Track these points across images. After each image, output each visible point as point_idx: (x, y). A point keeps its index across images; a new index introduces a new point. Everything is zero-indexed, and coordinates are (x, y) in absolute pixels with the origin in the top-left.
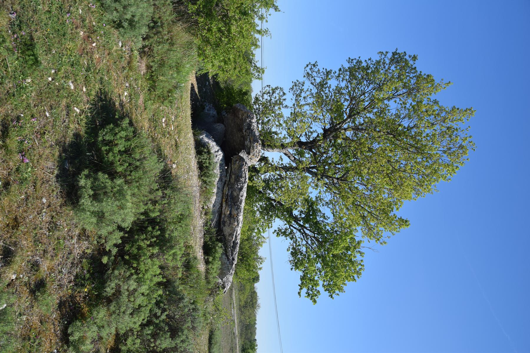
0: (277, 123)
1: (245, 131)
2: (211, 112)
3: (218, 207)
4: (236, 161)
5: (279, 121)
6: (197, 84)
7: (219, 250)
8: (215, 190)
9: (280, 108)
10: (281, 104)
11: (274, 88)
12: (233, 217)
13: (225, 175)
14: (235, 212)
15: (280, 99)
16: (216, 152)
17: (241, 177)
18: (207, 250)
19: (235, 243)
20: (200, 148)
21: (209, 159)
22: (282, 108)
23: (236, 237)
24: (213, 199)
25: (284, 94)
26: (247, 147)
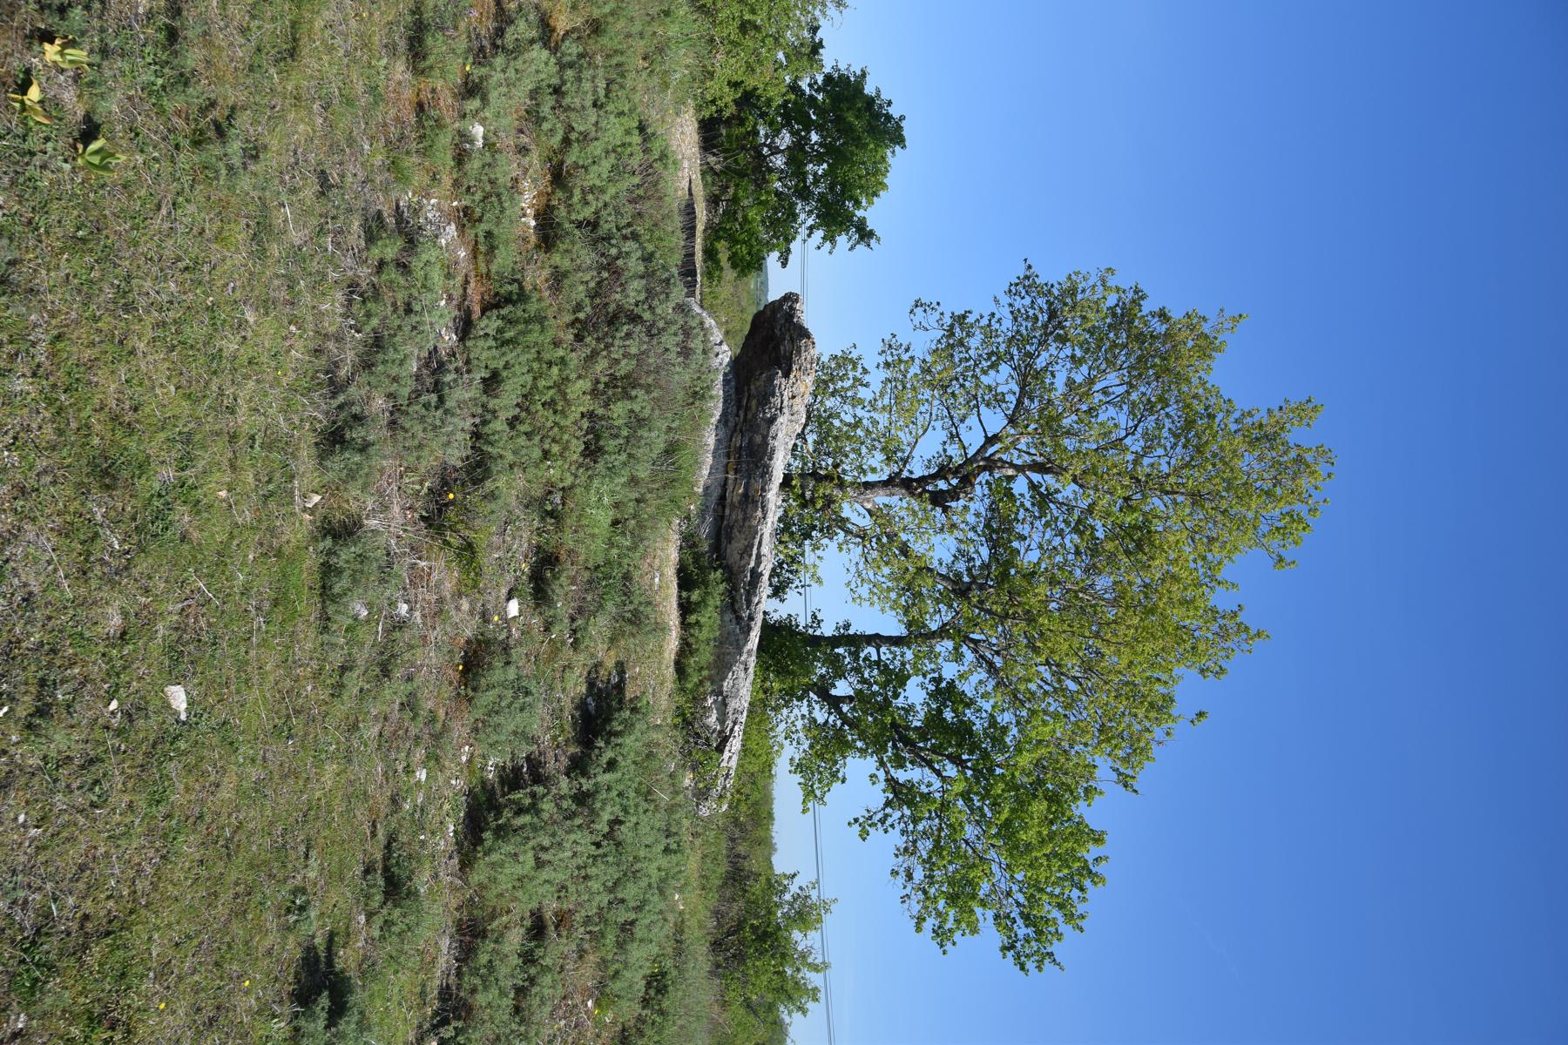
8: (711, 440)
18: (686, 581)
19: (756, 575)
23: (759, 556)
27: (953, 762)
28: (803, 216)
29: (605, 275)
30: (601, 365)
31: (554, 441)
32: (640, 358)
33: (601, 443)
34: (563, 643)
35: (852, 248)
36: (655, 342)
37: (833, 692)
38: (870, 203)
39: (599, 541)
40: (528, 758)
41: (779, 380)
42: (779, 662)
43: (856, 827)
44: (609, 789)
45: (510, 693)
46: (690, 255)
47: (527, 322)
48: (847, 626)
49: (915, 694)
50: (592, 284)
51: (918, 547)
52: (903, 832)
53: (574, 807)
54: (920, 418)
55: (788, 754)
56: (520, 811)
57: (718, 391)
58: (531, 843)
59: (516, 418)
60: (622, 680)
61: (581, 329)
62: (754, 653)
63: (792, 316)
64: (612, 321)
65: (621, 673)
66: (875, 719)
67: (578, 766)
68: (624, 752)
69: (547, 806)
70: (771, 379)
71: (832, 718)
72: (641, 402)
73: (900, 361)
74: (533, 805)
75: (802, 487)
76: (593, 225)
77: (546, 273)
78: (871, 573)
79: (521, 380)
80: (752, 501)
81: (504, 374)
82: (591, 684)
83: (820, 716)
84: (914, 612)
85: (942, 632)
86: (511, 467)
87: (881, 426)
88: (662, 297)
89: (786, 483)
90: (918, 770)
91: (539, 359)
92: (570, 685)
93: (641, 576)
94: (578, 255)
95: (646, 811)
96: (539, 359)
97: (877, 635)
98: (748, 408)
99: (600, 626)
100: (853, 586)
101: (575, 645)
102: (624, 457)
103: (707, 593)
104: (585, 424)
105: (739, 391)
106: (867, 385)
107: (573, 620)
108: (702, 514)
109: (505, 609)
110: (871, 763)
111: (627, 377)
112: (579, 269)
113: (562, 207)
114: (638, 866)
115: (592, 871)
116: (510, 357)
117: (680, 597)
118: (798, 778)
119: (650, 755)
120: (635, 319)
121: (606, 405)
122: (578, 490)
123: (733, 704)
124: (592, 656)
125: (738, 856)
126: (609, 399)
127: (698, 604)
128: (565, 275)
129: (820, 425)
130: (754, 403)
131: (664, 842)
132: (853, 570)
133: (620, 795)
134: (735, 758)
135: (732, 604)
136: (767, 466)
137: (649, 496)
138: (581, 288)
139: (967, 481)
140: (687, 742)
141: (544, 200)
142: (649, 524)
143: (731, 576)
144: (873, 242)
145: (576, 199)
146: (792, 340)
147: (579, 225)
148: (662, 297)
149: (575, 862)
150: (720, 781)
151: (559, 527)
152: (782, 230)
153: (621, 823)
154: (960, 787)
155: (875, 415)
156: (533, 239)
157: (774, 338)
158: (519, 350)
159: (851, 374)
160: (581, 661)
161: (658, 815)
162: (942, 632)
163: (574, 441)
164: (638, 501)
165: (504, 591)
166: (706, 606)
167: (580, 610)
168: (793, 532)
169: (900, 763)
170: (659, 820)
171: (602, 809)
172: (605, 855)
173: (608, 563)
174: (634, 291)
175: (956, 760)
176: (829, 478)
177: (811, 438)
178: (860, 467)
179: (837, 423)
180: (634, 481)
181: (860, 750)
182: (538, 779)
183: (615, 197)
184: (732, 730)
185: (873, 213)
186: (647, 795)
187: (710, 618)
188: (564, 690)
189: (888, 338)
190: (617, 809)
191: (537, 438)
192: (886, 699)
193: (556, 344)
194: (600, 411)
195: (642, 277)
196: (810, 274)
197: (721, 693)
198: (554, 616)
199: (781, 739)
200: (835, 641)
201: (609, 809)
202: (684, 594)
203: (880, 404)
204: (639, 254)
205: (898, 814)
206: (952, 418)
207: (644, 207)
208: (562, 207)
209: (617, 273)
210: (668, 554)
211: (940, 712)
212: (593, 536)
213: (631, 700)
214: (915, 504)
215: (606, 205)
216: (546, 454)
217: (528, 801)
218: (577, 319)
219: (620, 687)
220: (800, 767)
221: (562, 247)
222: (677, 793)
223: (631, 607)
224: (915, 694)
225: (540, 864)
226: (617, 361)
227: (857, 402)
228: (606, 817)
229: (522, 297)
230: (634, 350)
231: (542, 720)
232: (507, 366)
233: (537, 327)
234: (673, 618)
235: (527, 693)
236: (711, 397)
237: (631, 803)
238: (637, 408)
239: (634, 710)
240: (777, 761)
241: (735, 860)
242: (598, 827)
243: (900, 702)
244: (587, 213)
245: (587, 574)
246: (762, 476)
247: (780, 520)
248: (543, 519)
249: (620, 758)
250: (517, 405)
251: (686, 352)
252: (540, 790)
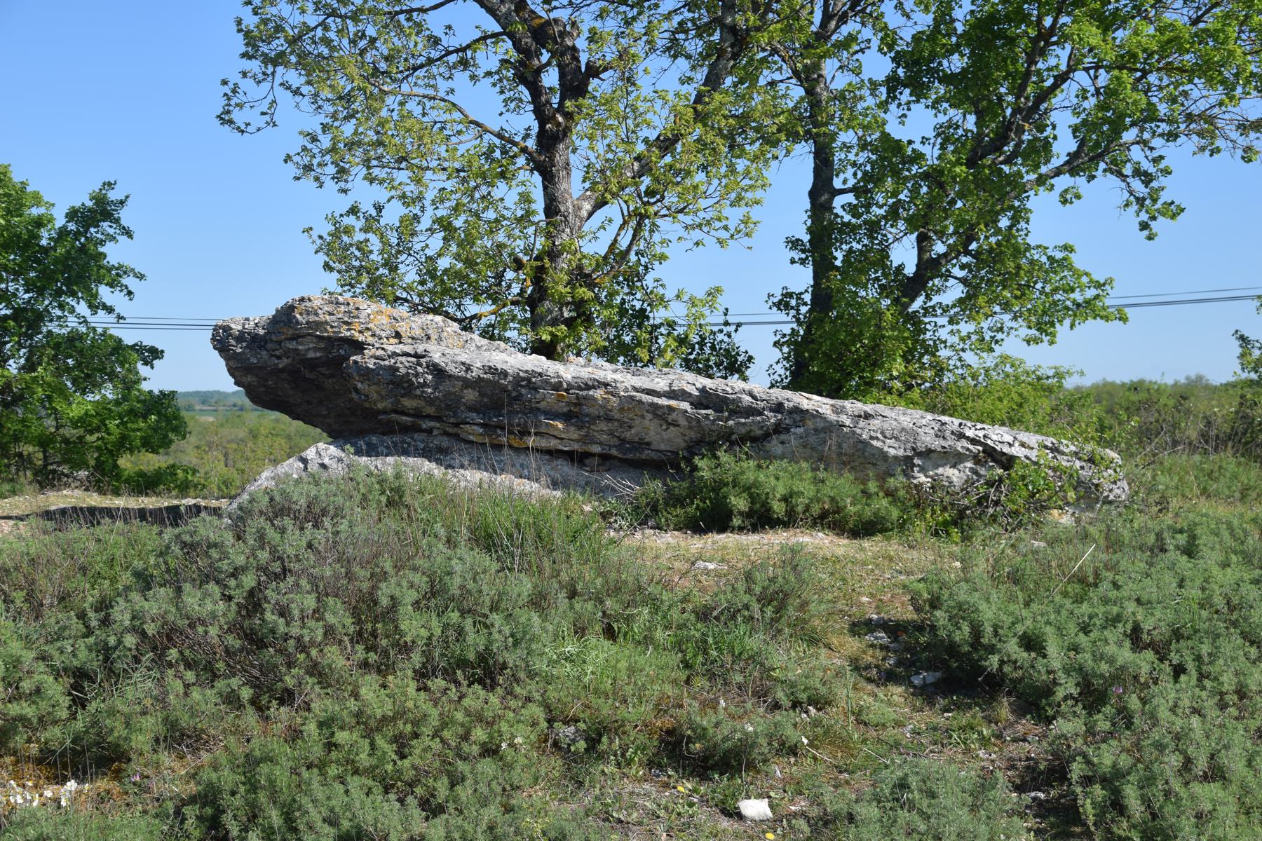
8: (472, 477)
13: (423, 436)
18: (715, 519)
19: (705, 399)
23: (672, 394)
27: (1043, 53)
28: (72, 322)
29: (173, 654)
30: (335, 658)
31: (465, 737)
32: (322, 592)
33: (471, 656)
34: (816, 723)
35: (128, 233)
36: (295, 566)
37: (910, 270)
38: (37, 199)
39: (641, 660)
40: (1020, 789)
41: (368, 360)
42: (856, 363)
43: (1159, 225)
44: (1075, 648)
45: (903, 815)
46: (142, 514)
47: (253, 787)
48: (794, 244)
49: (917, 125)
50: (190, 676)
51: (658, 122)
52: (1171, 136)
53: (1108, 709)
54: (434, 115)
55: (1017, 346)
56: (1117, 805)
57: (387, 465)
58: (1176, 786)
59: (424, 804)
60: (884, 625)
61: (270, 693)
62: (839, 402)
63: (255, 338)
64: (256, 641)
65: (869, 626)
66: (961, 195)
67: (1035, 702)
68: (1008, 620)
69: (1107, 757)
70: (366, 373)
71: (957, 272)
72: (402, 589)
73: (333, 150)
74: (1105, 781)
75: (554, 323)
76: (80, 678)
77: (166, 758)
78: (703, 203)
79: (357, 794)
80: (577, 406)
81: (346, 824)
82: (889, 677)
83: (953, 292)
84: (771, 126)
85: (809, 78)
86: (508, 809)
87: (449, 185)
88: (214, 554)
89: (548, 350)
90: (1055, 116)
91: (322, 766)
92: (890, 714)
93: (703, 590)
94: (134, 706)
95: (1116, 586)
96: (322, 766)
97: (813, 194)
98: (418, 414)
99: (787, 660)
100: (724, 235)
101: (821, 703)
102: (496, 619)
103: (735, 483)
104: (438, 683)
105: (387, 429)
106: (379, 208)
107: (777, 706)
108: (600, 492)
109: (758, 823)
110: (1041, 204)
111: (356, 613)
112: (161, 700)
113: (44, 736)
114: (1219, 602)
115: (1228, 682)
116: (315, 816)
117: (741, 529)
118: (1062, 330)
119: (1015, 578)
120: (254, 603)
121: (406, 649)
122: (552, 695)
123: (928, 439)
124: (839, 674)
125: (1205, 436)
126: (395, 644)
127: (753, 499)
128: (171, 725)
129: (446, 291)
130: (408, 403)
131: (1173, 554)
132: (697, 235)
133: (1085, 629)
134: (1024, 436)
135: (754, 440)
136: (518, 380)
137: (564, 576)
138: (196, 694)
139: (543, 33)
140: (994, 518)
141: (29, 768)
142: (613, 575)
143: (705, 442)
144: (113, 195)
145: (28, 710)
146: (296, 338)
147: (79, 703)
148: (214, 554)
149: (1212, 712)
150: (1064, 462)
151: (616, 728)
152: (106, 359)
153: (1137, 629)
154: (1092, 34)
155: (430, 195)
156: (103, 784)
157: (294, 370)
158: (305, 801)
159: (359, 236)
160: (848, 693)
161: (1124, 564)
162: (809, 78)
163: (466, 702)
164: (573, 594)
165: (725, 823)
166: (756, 484)
167: (761, 694)
168: (632, 339)
169: (1042, 149)
170: (1132, 564)
171: (1111, 661)
172: (1198, 658)
173: (678, 645)
174: (207, 605)
175: (1042, 42)
176: (539, 276)
177: (471, 308)
178: (519, 220)
179: (444, 263)
180: (538, 602)
181: (1015, 220)
182: (1057, 773)
183: (27, 641)
184: (973, 441)
185: (58, 195)
186: (1085, 583)
187: (777, 479)
188: (899, 724)
189: (291, 170)
190: (1112, 635)
191: (462, 766)
192: (926, 176)
193: (295, 735)
194: (417, 659)
195: (179, 590)
196: (178, 310)
197: (908, 461)
198: (770, 737)
199: (990, 360)
200: (822, 267)
201: (1111, 649)
202: (736, 522)
203: (410, 189)
204: (135, 596)
205: (1136, 153)
206: (430, 61)
207: (47, 591)
208: (44, 736)
209: (170, 634)
210: (665, 545)
211: (947, 79)
212: (631, 671)
213: (918, 610)
214: (583, 126)
215: (43, 658)
216: (489, 751)
217: (1098, 791)
218: (254, 702)
219: (894, 629)
220: (1044, 326)
221: (119, 731)
222: (1085, 537)
223: (756, 607)
224: (917, 125)
225: (1216, 773)
226: (329, 631)
227: (408, 226)
228: (1125, 655)
229: (209, 798)
230: (310, 602)
231: (951, 761)
232: (331, 821)
233: (264, 769)
234: (775, 539)
235: (903, 785)
236: (398, 476)
237: (1101, 610)
238: (412, 596)
239: (935, 603)
240: (1030, 364)
241: (1211, 440)
242: (1145, 669)
243: (931, 153)
244: (57, 690)
245: (700, 682)
246: (535, 389)
247: (612, 360)
248: (601, 757)
249: (1020, 629)
250: (401, 801)
251: (314, 515)
252: (1077, 769)
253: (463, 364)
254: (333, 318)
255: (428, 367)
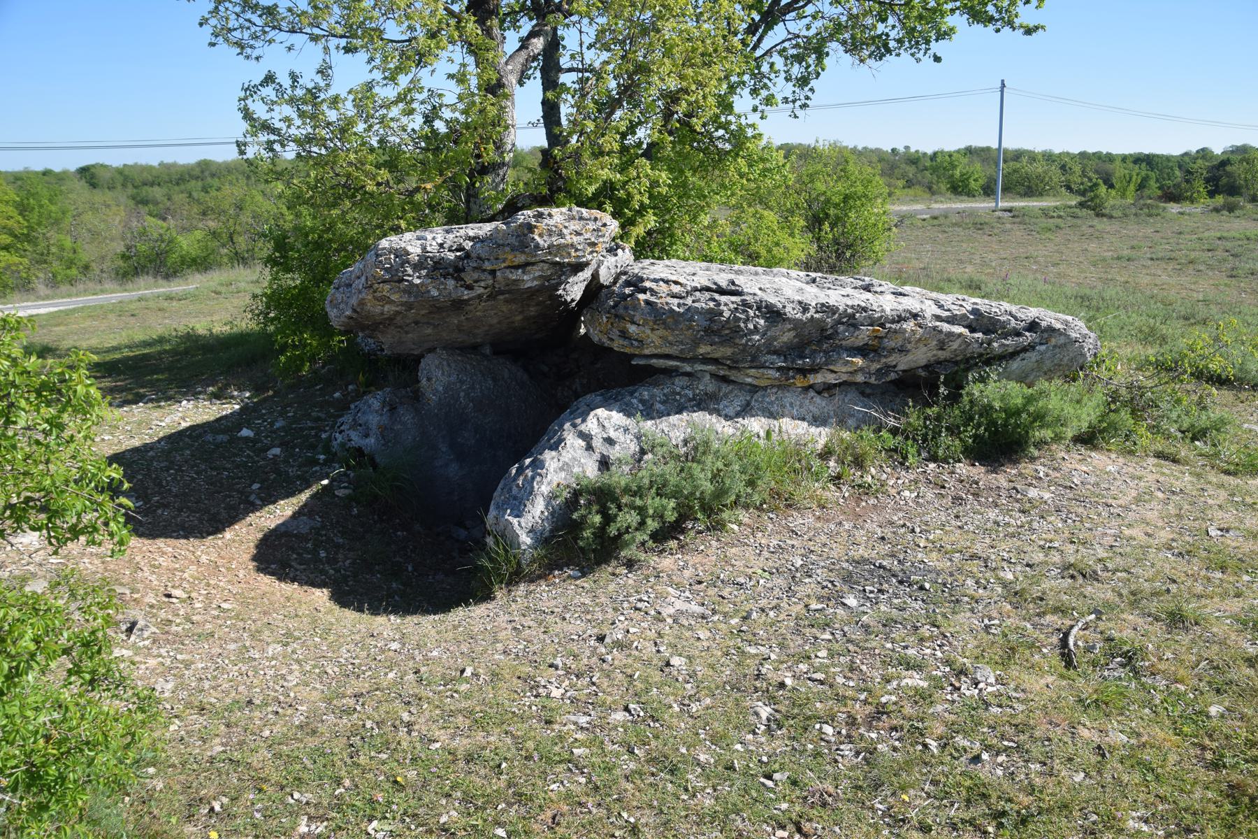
0: (395, 112)
1: (469, 287)
2: (374, 420)
3: (819, 404)
4: (624, 334)
5: (387, 105)
6: (253, 508)
7: (995, 391)
8: (756, 425)
9: (335, 101)
10: (313, 94)
11: (245, 126)
12: (879, 337)
13: (683, 381)
14: (866, 331)
15: (292, 101)
16: (589, 448)
17: (714, 314)
20: (585, 540)
21: (639, 492)
22: (332, 92)
24: (793, 428)
25: (269, 79)
26: (548, 279)
253: (800, 303)
254: (580, 239)
255: (759, 308)
